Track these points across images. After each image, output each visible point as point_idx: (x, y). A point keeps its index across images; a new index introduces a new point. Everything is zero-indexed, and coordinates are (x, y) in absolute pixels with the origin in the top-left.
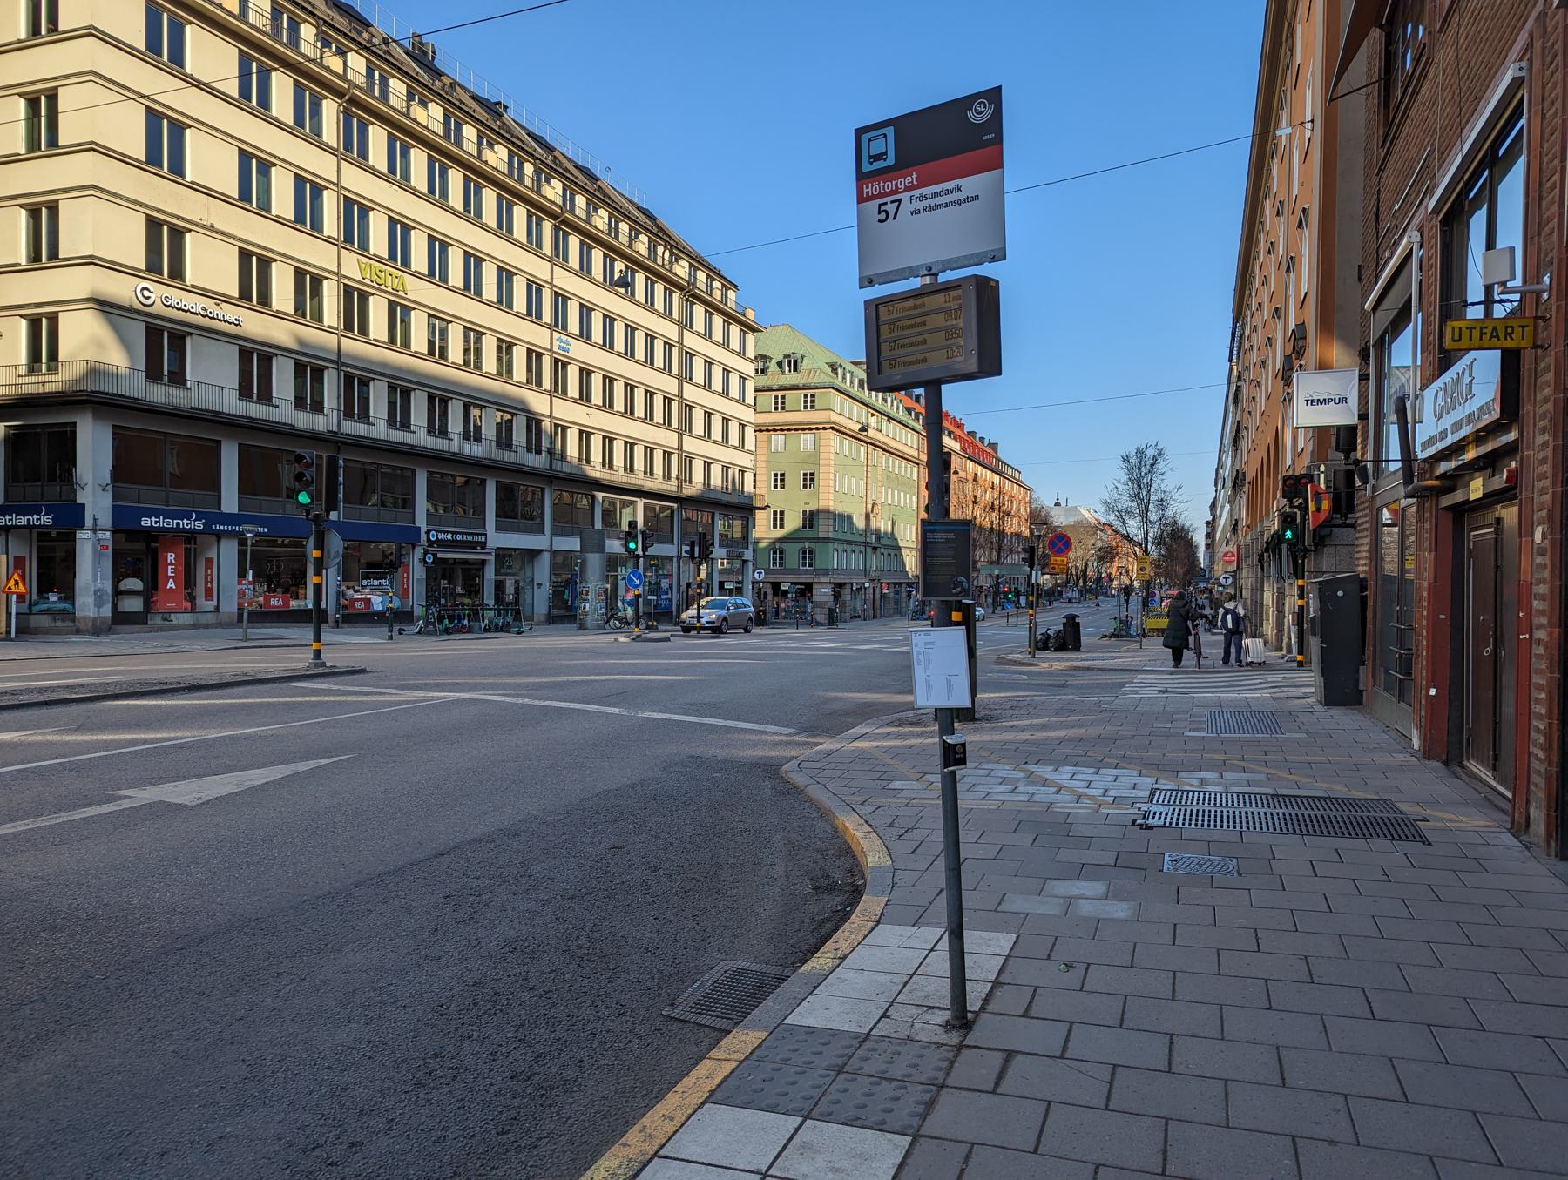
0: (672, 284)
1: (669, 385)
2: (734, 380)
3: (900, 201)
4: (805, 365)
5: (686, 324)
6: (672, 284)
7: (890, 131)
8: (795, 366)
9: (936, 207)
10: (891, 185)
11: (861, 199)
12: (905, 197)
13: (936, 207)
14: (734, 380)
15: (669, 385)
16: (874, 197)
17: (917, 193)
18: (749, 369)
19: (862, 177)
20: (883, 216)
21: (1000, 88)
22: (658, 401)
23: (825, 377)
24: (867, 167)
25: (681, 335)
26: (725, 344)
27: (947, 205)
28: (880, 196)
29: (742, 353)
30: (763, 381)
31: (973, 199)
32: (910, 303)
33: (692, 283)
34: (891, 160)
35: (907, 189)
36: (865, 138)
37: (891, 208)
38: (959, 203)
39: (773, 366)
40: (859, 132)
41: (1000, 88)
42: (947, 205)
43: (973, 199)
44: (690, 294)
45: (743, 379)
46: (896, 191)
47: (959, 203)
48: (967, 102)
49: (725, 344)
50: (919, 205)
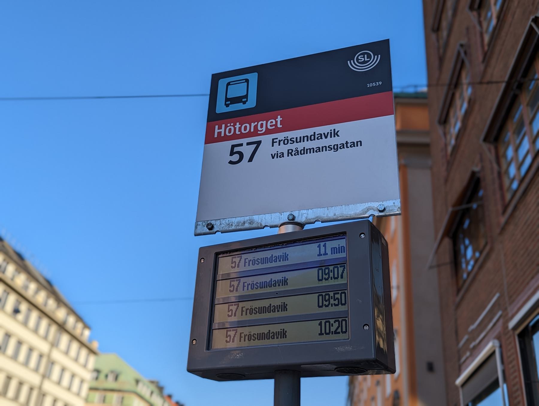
0: (52, 320)
1: (34, 379)
2: (76, 382)
3: (259, 143)
4: (121, 378)
5: (54, 344)
6: (52, 320)
7: (253, 78)
8: (116, 378)
9: (305, 151)
10: (250, 127)
11: (210, 139)
12: (266, 140)
13: (305, 151)
14: (76, 382)
15: (34, 379)
16: (226, 138)
17: (281, 136)
18: (88, 376)
19: (214, 117)
20: (236, 157)
21: (387, 41)
22: (25, 390)
23: (130, 386)
24: (221, 108)
25: (50, 351)
26: (76, 360)
27: (319, 150)
28: (235, 137)
29: (85, 366)
30: (95, 384)
31: (353, 145)
32: (267, 254)
33: (65, 322)
34: (252, 103)
35: (268, 132)
36: (222, 83)
37: (247, 150)
38: (336, 148)
39: (102, 376)
40: (216, 78)
41: (387, 41)
42: (319, 150)
43: (353, 145)
44: (62, 327)
45: (82, 381)
46: (256, 133)
47: (336, 148)
48: (350, 52)
49: (76, 360)
50: (284, 148)
